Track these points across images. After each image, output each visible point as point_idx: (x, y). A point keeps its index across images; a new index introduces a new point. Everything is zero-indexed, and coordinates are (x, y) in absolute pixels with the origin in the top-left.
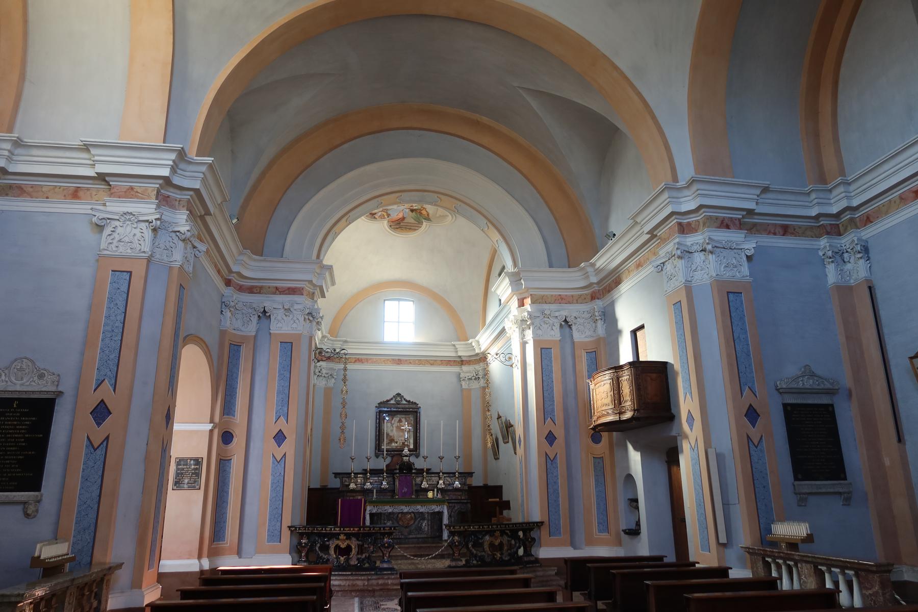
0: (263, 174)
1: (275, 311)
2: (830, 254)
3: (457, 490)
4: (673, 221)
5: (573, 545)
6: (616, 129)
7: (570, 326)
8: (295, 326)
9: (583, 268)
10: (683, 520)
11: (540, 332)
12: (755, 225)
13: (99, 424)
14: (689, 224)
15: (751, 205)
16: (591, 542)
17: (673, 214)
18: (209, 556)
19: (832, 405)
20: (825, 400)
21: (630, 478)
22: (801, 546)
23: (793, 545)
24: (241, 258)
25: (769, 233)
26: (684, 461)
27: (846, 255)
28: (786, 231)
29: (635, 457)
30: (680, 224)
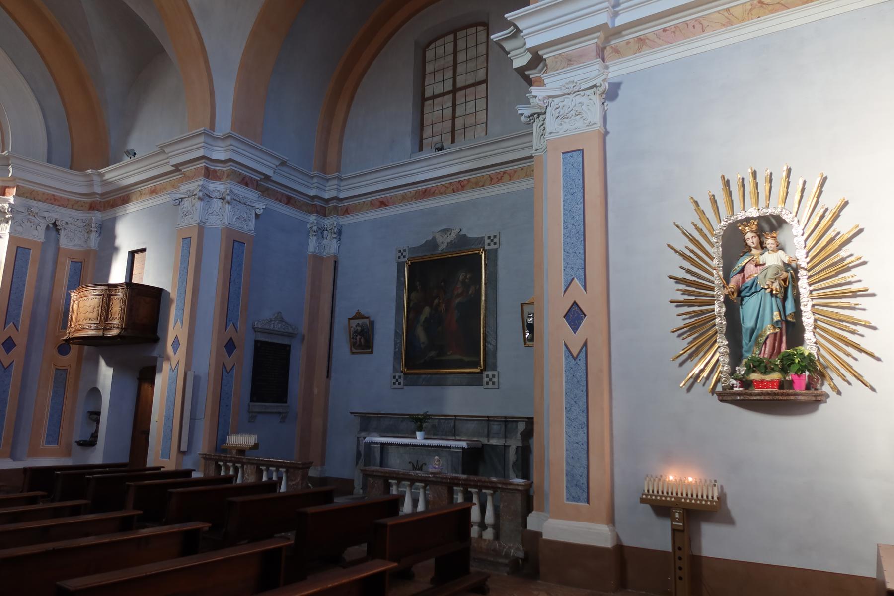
2: (315, 229)
4: (202, 164)
5: (13, 457)
6: (161, 50)
7: (58, 231)
9: (89, 175)
10: (147, 433)
11: (19, 229)
12: (267, 189)
14: (215, 171)
15: (269, 173)
16: (34, 453)
17: (203, 157)
19: (289, 346)
20: (284, 341)
21: (95, 393)
22: (247, 453)
23: (241, 451)
25: (276, 199)
26: (159, 380)
27: (325, 233)
28: (289, 201)
29: (106, 373)
30: (207, 169)
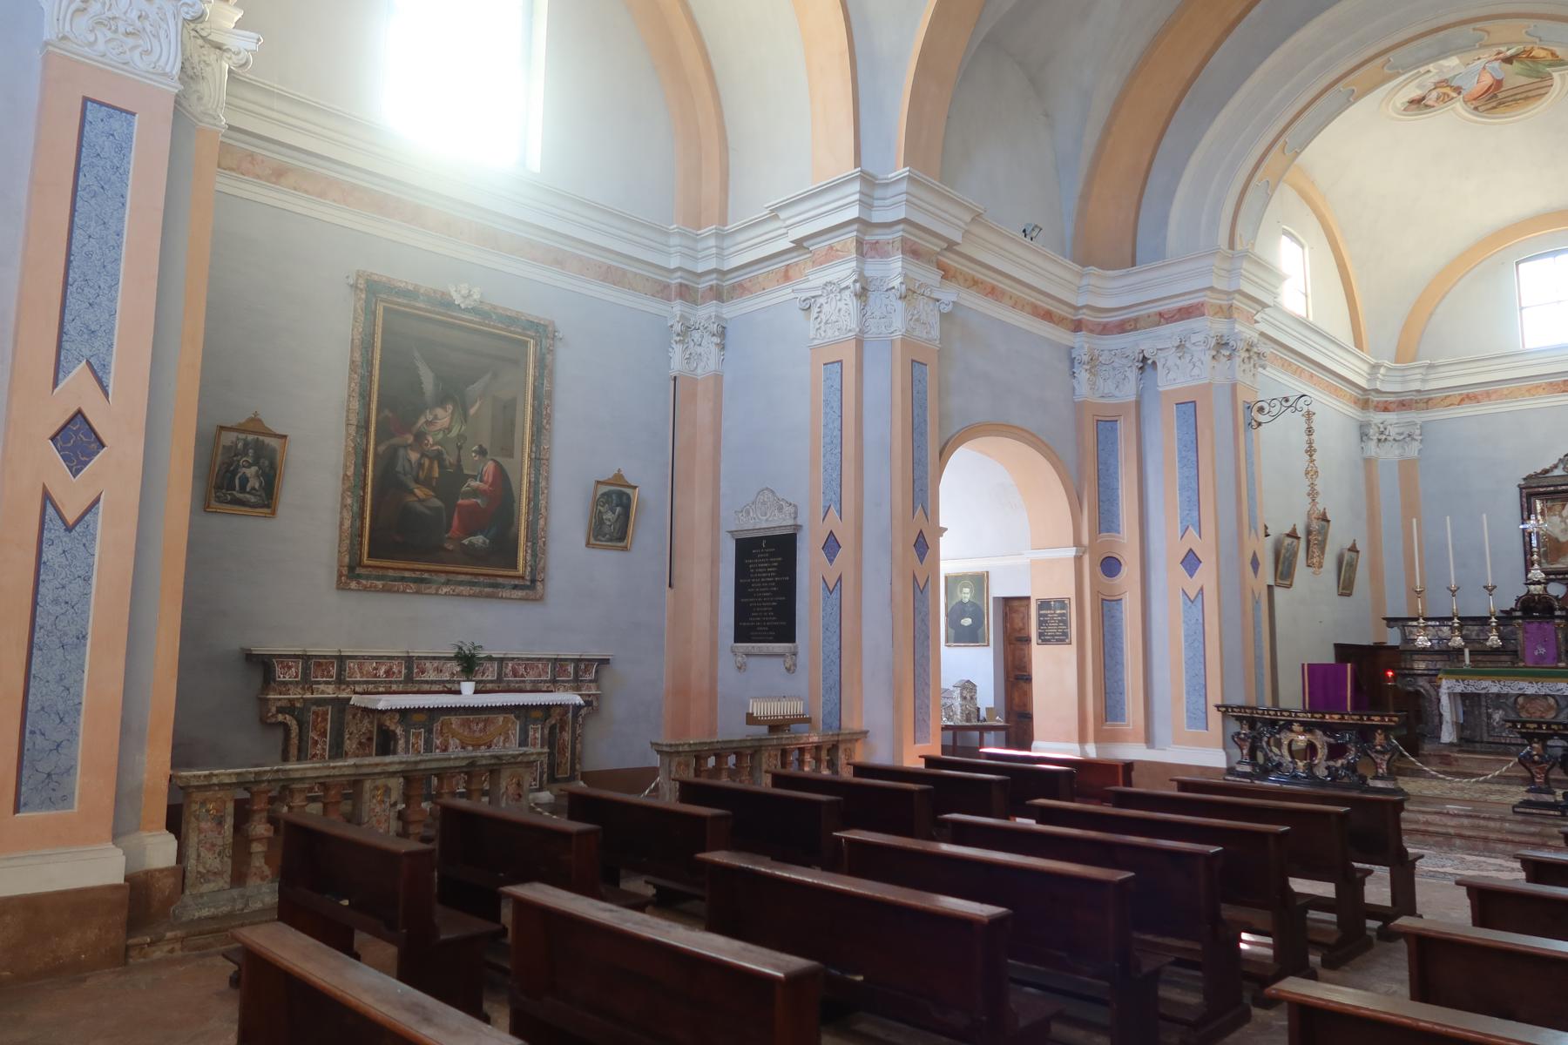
0: (1107, 129)
1: (1161, 354)
3: (1495, 651)
8: (1196, 371)
13: (831, 561)
18: (1098, 740)
24: (1084, 282)
